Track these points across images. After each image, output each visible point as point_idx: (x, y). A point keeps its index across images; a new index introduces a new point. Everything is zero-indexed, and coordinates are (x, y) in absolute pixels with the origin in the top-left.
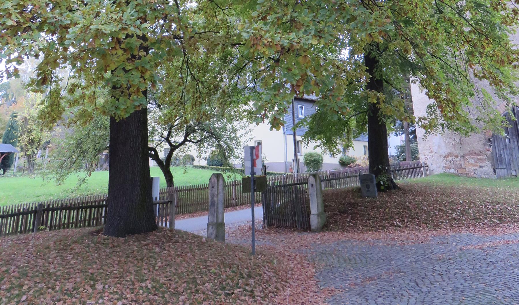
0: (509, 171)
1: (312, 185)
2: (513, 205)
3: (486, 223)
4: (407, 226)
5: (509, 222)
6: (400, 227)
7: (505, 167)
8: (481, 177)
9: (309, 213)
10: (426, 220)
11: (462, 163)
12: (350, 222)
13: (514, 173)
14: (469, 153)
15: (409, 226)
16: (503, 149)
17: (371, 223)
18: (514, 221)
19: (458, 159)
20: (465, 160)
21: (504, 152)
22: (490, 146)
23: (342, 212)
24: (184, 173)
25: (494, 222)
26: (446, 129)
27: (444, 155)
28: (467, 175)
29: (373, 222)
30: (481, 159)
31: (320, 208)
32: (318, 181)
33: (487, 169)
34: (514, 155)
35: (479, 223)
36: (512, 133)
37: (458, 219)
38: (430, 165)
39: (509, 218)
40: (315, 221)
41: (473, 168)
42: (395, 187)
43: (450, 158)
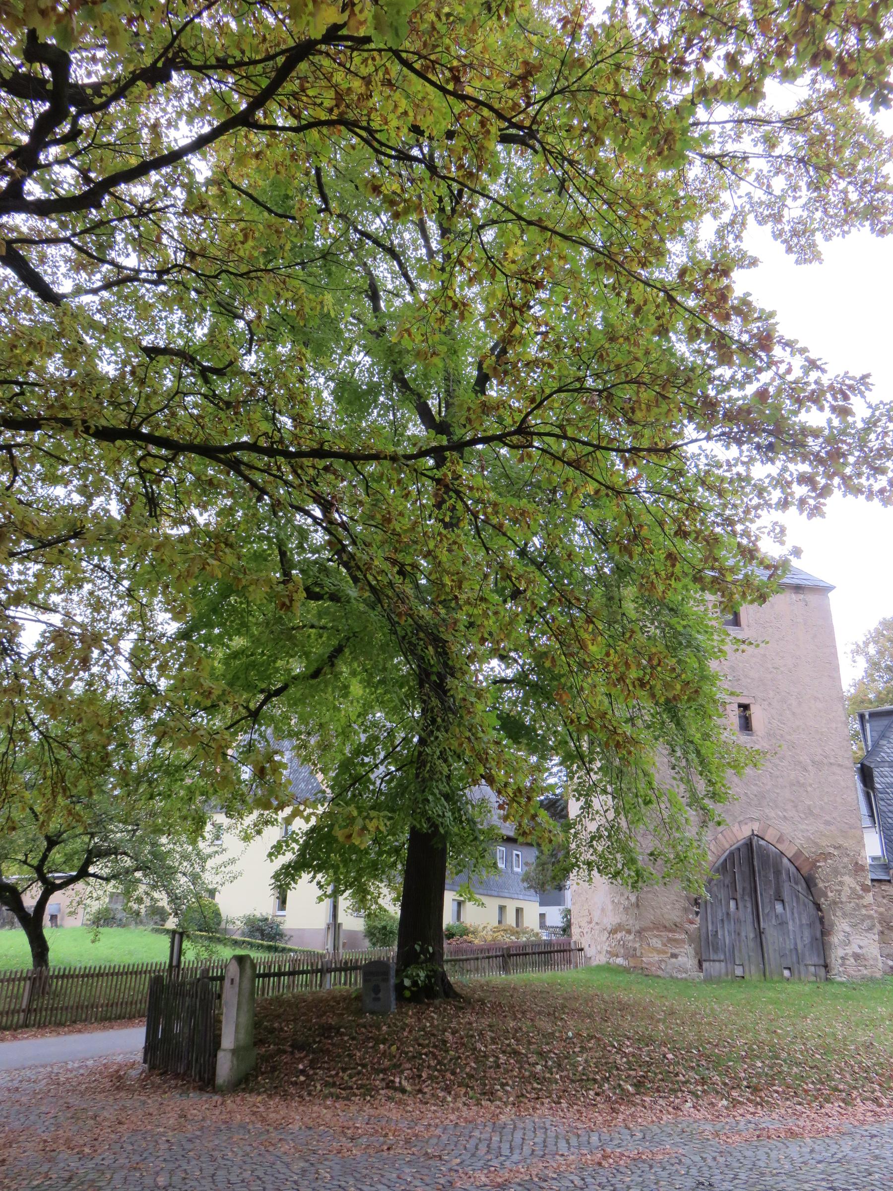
0: (729, 966)
1: (232, 980)
2: (683, 1048)
3: (604, 1091)
4: (420, 1091)
5: (659, 1091)
6: (403, 1091)
7: (722, 957)
8: (672, 977)
9: (217, 1044)
10: (472, 1076)
11: (637, 945)
12: (302, 1072)
13: (739, 971)
14: (651, 925)
15: (426, 1090)
16: (722, 920)
17: (346, 1078)
18: (671, 1090)
19: (631, 937)
20: (641, 939)
21: (723, 927)
22: (697, 913)
23: (298, 1046)
24: (93, 942)
25: (623, 1090)
26: (595, 872)
27: (609, 927)
28: (644, 972)
29: (351, 1077)
30: (675, 940)
31: (242, 1036)
32: (248, 971)
33: (685, 959)
34: (743, 934)
35: (588, 1090)
36: (744, 889)
37: (544, 1078)
38: (586, 948)
39: (662, 1080)
40: (225, 1066)
41: (656, 957)
42: (449, 992)
43: (619, 936)
